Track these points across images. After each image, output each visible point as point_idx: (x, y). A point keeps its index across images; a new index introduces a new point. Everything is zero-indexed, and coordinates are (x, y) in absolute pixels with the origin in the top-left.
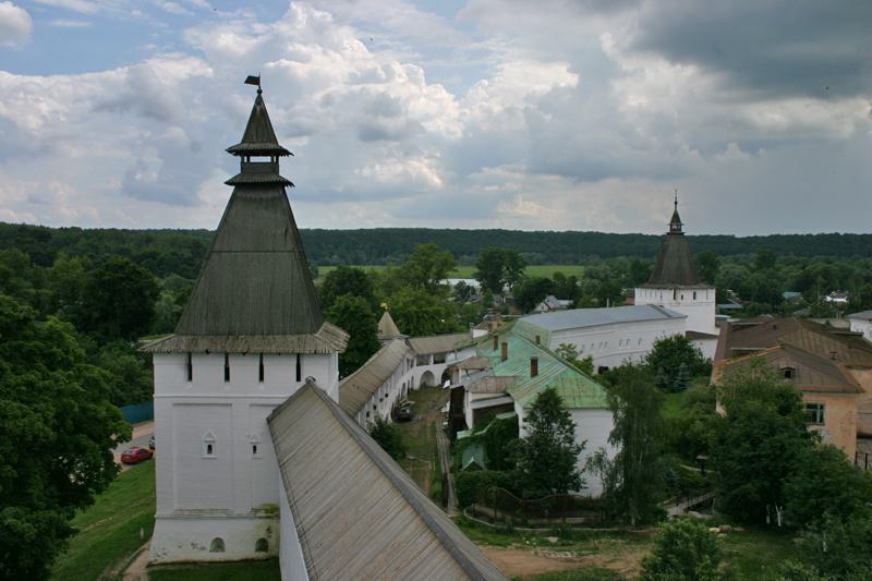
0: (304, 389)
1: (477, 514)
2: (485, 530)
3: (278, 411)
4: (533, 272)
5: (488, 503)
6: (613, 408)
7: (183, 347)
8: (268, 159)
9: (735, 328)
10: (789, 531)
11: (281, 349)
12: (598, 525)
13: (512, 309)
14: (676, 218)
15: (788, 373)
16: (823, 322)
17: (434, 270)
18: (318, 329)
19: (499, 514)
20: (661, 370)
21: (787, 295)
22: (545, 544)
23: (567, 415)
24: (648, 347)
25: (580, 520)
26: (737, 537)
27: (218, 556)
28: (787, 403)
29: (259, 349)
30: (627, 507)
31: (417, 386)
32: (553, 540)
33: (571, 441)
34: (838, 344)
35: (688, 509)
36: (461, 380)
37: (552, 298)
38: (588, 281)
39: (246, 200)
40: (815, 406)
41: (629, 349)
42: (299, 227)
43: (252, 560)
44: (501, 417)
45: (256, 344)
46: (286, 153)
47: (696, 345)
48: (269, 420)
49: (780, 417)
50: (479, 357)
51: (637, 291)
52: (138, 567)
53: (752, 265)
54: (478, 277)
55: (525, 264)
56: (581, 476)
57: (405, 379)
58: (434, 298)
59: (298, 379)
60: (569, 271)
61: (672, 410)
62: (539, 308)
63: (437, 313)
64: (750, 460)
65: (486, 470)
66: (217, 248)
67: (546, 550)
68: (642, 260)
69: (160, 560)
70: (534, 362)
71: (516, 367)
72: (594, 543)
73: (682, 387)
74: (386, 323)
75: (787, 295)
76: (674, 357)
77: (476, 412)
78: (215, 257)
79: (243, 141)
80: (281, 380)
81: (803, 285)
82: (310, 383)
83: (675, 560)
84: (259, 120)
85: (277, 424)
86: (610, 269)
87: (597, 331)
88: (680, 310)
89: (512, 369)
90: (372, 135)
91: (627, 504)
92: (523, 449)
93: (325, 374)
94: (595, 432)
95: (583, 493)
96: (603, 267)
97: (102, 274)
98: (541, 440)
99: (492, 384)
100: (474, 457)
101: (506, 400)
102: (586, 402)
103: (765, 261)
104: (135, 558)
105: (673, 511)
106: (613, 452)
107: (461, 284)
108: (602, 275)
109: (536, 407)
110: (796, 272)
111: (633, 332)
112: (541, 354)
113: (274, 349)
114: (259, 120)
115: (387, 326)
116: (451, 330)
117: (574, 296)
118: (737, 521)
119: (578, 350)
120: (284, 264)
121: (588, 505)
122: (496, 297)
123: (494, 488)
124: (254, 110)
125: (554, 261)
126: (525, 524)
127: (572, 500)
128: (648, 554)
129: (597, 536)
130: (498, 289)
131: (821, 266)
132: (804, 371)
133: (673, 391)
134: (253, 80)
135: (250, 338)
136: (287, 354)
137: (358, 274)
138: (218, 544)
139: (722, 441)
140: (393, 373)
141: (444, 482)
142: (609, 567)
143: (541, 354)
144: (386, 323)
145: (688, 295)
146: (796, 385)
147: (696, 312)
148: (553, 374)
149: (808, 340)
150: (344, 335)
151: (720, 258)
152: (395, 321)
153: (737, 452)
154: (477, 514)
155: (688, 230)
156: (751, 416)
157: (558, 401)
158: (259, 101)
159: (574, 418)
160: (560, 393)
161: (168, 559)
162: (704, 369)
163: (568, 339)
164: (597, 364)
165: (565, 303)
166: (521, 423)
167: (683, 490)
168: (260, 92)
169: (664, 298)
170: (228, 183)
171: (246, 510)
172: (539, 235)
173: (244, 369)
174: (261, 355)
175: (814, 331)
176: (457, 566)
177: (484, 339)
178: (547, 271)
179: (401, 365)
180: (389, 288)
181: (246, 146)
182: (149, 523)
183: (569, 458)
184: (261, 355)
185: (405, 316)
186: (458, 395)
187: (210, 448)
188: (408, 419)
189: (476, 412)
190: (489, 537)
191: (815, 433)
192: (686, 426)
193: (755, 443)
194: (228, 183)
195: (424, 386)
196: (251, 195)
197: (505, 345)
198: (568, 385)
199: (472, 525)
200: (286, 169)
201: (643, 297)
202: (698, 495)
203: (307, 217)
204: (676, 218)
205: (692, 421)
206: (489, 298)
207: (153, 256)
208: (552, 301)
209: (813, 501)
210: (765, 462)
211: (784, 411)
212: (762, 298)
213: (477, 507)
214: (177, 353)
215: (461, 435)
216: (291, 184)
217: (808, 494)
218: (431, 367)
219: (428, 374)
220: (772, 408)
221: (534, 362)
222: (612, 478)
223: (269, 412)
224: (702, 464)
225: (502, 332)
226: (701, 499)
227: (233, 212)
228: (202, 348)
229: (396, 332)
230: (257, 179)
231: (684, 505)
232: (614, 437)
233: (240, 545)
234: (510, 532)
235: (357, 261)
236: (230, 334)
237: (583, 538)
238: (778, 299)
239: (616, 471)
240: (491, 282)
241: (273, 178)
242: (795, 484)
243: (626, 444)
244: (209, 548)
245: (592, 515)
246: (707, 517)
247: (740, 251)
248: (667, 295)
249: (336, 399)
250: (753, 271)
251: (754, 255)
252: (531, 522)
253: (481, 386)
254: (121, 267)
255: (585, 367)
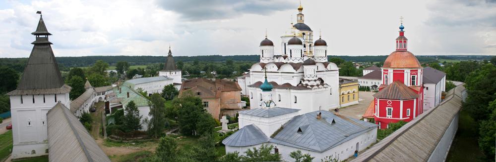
0: (57, 104)
1: (112, 138)
2: (114, 142)
3: (50, 111)
4: (132, 68)
5: (116, 134)
6: (150, 105)
7: (19, 93)
8: (44, 36)
9: (186, 82)
10: (198, 137)
11: (50, 93)
12: (148, 139)
13: (126, 78)
14: (170, 51)
15: (199, 94)
16: (209, 79)
17: (102, 68)
18: (61, 86)
19: (119, 137)
20: (166, 94)
21: (201, 72)
22: (131, 145)
23: (137, 108)
24: (163, 88)
25: (141, 138)
26: (184, 140)
27: (34, 155)
28: (198, 102)
29: (43, 93)
30: (155, 132)
31: (97, 101)
32: (134, 144)
33: (138, 115)
34: (212, 85)
35: (172, 133)
36: (108, 99)
37: (137, 75)
38: (148, 70)
39: (37, 49)
40: (206, 102)
41: (158, 88)
42: (55, 56)
43: (44, 156)
44: (119, 109)
45: (42, 92)
46: (50, 34)
47: (176, 87)
48: (47, 114)
49: (195, 106)
50: (114, 92)
51: (160, 72)
52: (9, 160)
53: (193, 64)
54: (117, 69)
55: (130, 65)
56: (142, 125)
57: (94, 99)
58: (103, 76)
59: (56, 101)
60: (142, 67)
61: (168, 105)
62: (133, 78)
63: (103, 80)
64: (187, 118)
65: (115, 125)
66: (29, 63)
67: (132, 147)
68: (163, 64)
69: (15, 158)
70: (128, 93)
71: (123, 96)
72: (145, 144)
73: (172, 98)
74: (88, 84)
75: (201, 72)
76: (170, 91)
77: (112, 108)
78: (28, 66)
79: (36, 31)
80: (50, 102)
81: (206, 69)
82: (59, 102)
83: (164, 148)
84: (41, 24)
85: (49, 115)
86: (151, 66)
87: (148, 84)
88: (171, 77)
89: (123, 96)
90: (87, 30)
91: (154, 133)
92: (125, 119)
93: (65, 100)
94: (145, 113)
95: (142, 130)
96: (152, 65)
97: (348, 67)
98: (130, 116)
99: (116, 100)
100: (112, 121)
101: (120, 105)
102: (143, 104)
103: (196, 63)
104: (7, 159)
105: (168, 133)
106: (150, 118)
107: (112, 71)
108: (152, 68)
109: (128, 106)
110: (204, 66)
111: (158, 84)
112: (130, 91)
113: (47, 93)
114: (41, 24)
115: (88, 85)
116: (108, 85)
117: (143, 74)
118: (185, 135)
119: (143, 89)
120: (51, 68)
121: (144, 133)
122: (122, 75)
123: (117, 130)
124: (40, 21)
125: (139, 64)
126: (126, 140)
127: (140, 132)
128: (157, 146)
129: (146, 142)
130: (122, 73)
131: (210, 64)
132: (203, 93)
133: (170, 100)
134: (39, 12)
135: (40, 90)
136: (30, 95)
137: (80, 70)
138: (34, 152)
139: (180, 113)
140: (89, 98)
141: (103, 129)
142: (149, 150)
143: (130, 91)
144: (88, 84)
145: (174, 73)
146: (200, 97)
147: (176, 78)
148: (133, 97)
149: (205, 84)
150: (70, 88)
151: (184, 63)
152: (90, 83)
153: (184, 116)
154: (112, 138)
155: (173, 55)
156: (188, 106)
157: (134, 104)
158: (41, 19)
159: (139, 109)
160: (135, 102)
161: (18, 158)
162: (177, 93)
163: (140, 86)
164: (148, 93)
165: (141, 76)
166: (124, 111)
167: (170, 127)
168: (41, 16)
169: (167, 74)
170: (32, 43)
171: (42, 141)
172: (134, 57)
173: (39, 100)
174: (44, 95)
175: (206, 82)
176: (85, 156)
177: (116, 87)
178: (136, 67)
179: (91, 96)
180: (89, 73)
181: (37, 32)
182: (12, 147)
183: (138, 120)
184: (44, 95)
185: (94, 81)
186: (107, 103)
187: (29, 123)
188: (94, 111)
189: (112, 108)
190: (116, 144)
191: (205, 110)
192: (172, 109)
193: (189, 113)
194: (32, 43)
195: (99, 101)
196: (39, 47)
197: (120, 89)
198: (137, 100)
199: (111, 141)
200: (50, 39)
201: (161, 74)
202: (175, 128)
203: (57, 53)
204: (170, 51)
205: (174, 108)
206: (120, 75)
207: (19, 66)
208: (137, 75)
209: (203, 128)
210: (192, 118)
211: (196, 104)
212: (195, 73)
213: (112, 136)
214: (18, 95)
215: (108, 115)
216: (51, 44)
217: (202, 127)
218: (101, 96)
219: (100, 98)
220: (194, 103)
221: (128, 93)
222: (150, 125)
223: (47, 112)
224: (176, 120)
225: (120, 85)
226: (176, 129)
227: (34, 52)
228: (26, 94)
229: (91, 86)
230: (41, 42)
231: (171, 132)
232: (150, 114)
233: (40, 152)
234: (121, 142)
235: (82, 66)
236: (34, 89)
237: (142, 142)
238: (199, 73)
239: (151, 123)
240: (120, 71)
241: (46, 42)
242: (199, 124)
243: (154, 115)
244: (31, 153)
245: (145, 136)
246: (177, 134)
247: (189, 60)
248: (168, 73)
249: (69, 107)
250: (193, 66)
251: (193, 62)
252: (128, 139)
253: (113, 101)
254: (6, 70)
255: (144, 95)
